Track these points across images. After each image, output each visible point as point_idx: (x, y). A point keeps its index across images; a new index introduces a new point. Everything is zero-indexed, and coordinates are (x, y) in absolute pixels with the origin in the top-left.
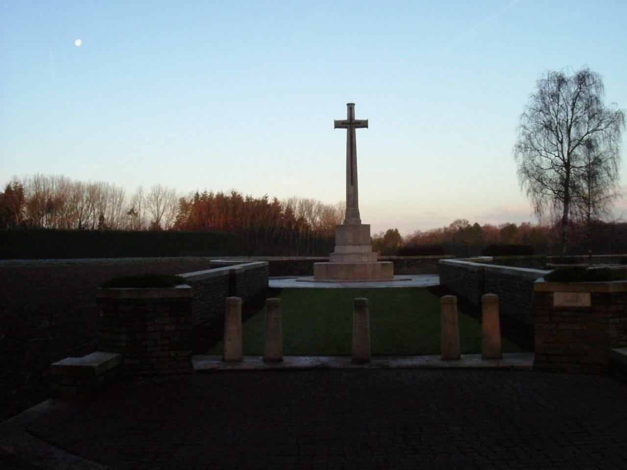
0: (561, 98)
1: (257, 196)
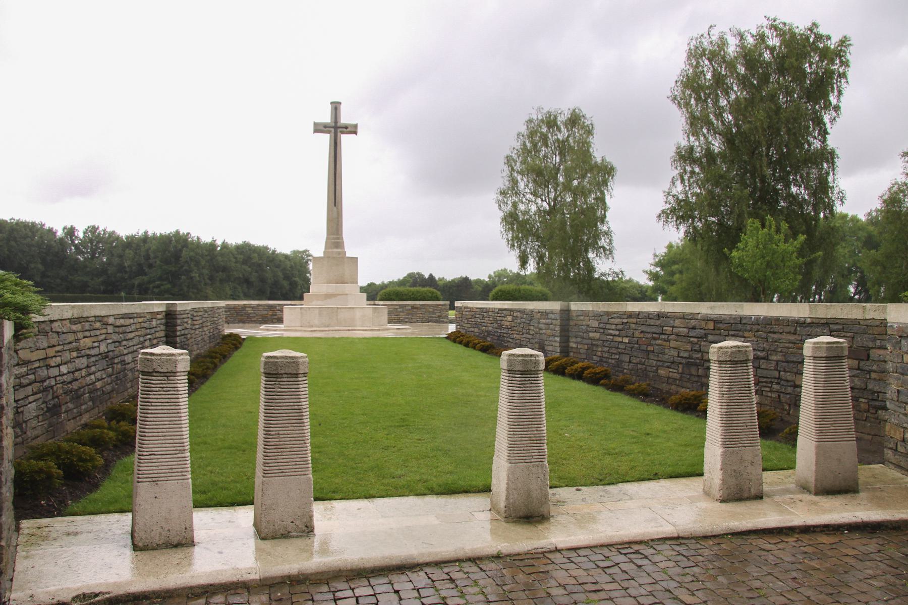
1: (206, 239)
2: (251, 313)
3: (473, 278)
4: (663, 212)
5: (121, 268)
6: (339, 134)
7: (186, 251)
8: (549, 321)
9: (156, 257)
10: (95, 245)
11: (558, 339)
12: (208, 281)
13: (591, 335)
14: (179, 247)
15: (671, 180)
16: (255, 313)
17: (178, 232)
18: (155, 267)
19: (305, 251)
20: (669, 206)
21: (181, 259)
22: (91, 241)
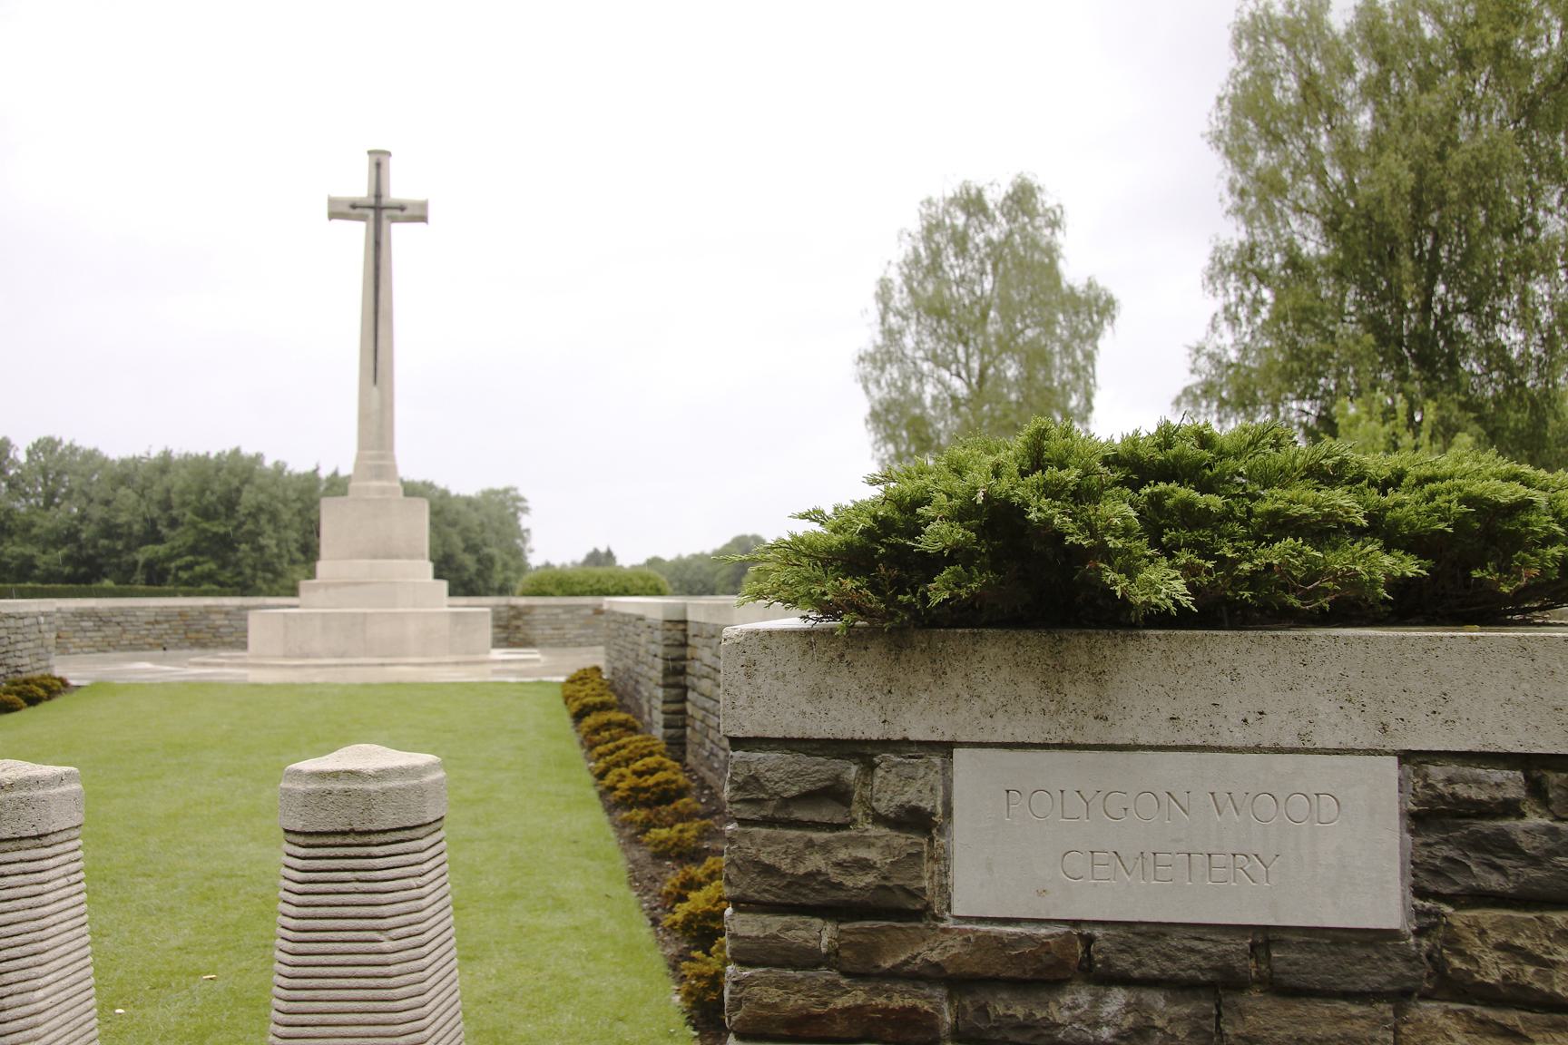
2: (221, 626)
4: (1187, 391)
5: (109, 530)
6: (385, 222)
7: (251, 492)
9: (184, 504)
10: (53, 480)
12: (299, 556)
14: (235, 483)
15: (1208, 321)
16: (232, 626)
17: (236, 452)
18: (182, 524)
19: (506, 491)
20: (1196, 379)
21: (237, 508)
22: (44, 471)
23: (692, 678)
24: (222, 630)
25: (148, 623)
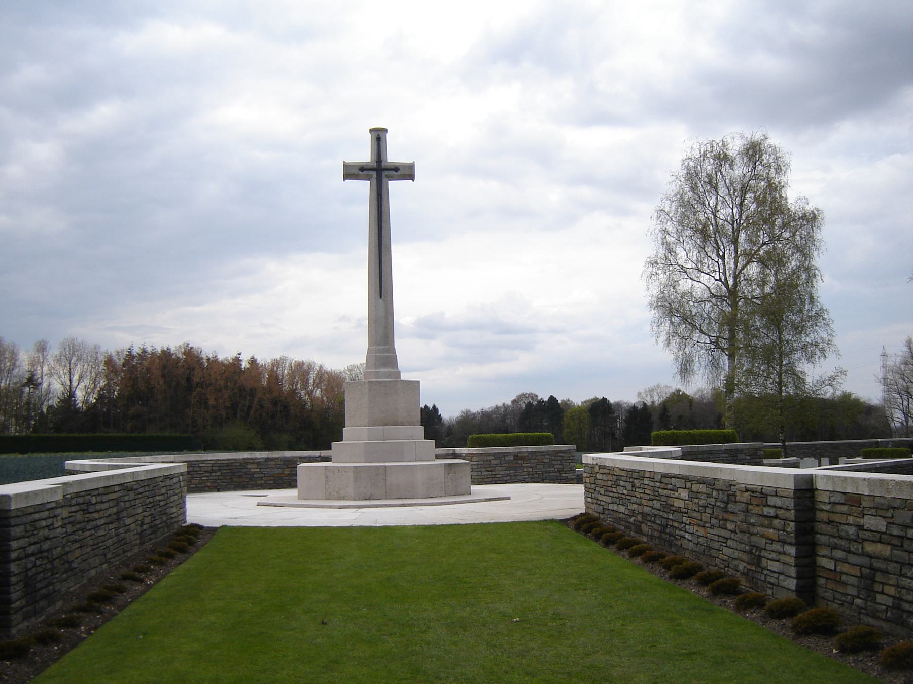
0: (721, 185)
1: (225, 355)
2: (254, 473)
3: (612, 400)
6: (384, 180)
8: (772, 512)
11: (792, 550)
13: (870, 548)
23: (818, 536)
24: (255, 476)
25: (206, 472)
